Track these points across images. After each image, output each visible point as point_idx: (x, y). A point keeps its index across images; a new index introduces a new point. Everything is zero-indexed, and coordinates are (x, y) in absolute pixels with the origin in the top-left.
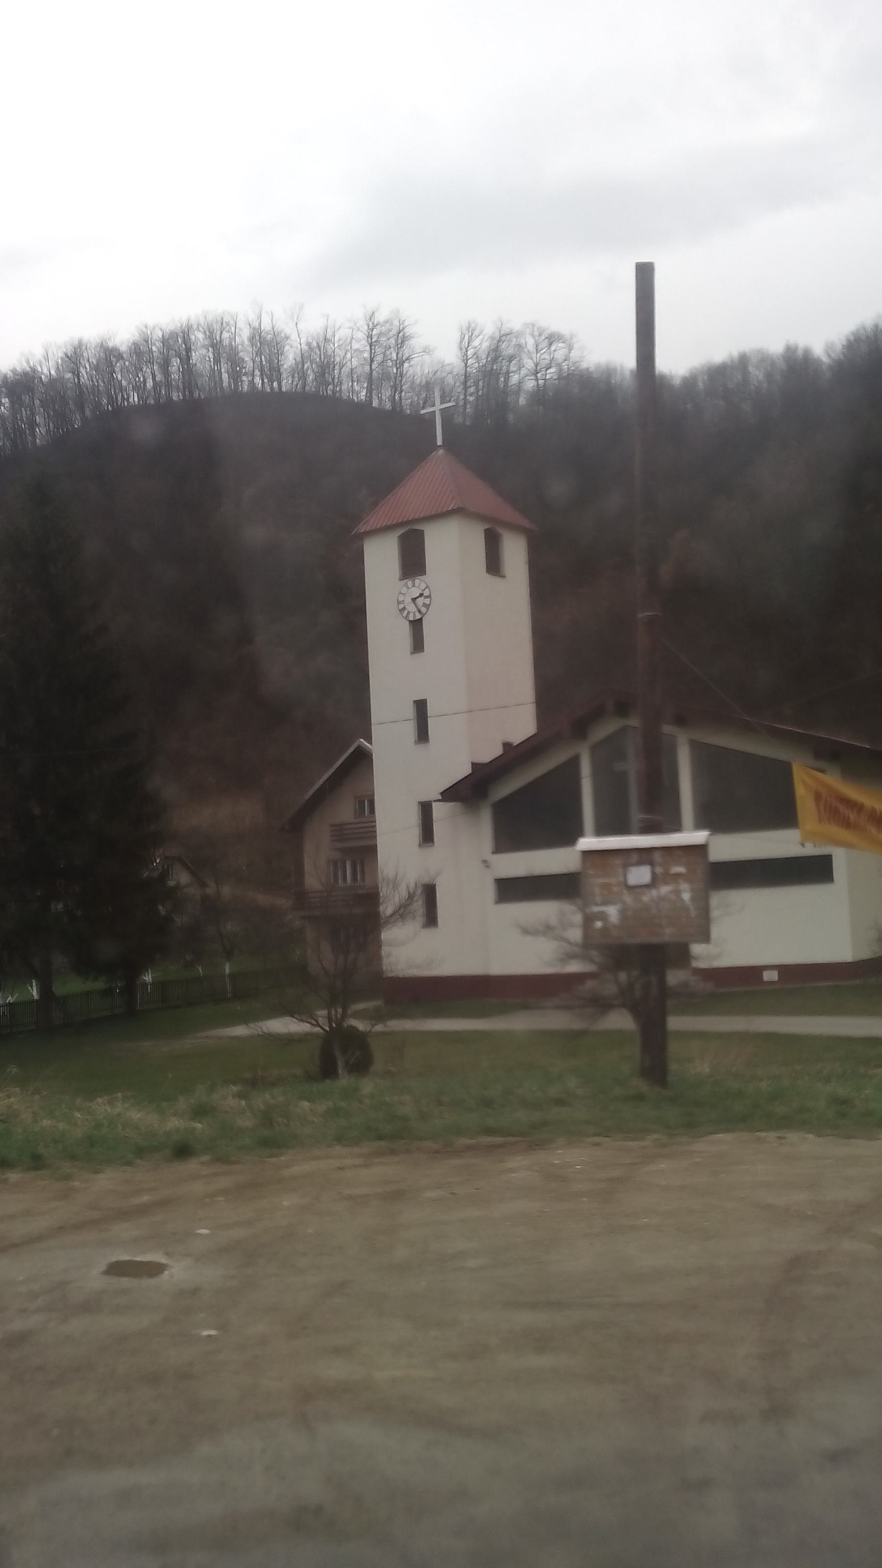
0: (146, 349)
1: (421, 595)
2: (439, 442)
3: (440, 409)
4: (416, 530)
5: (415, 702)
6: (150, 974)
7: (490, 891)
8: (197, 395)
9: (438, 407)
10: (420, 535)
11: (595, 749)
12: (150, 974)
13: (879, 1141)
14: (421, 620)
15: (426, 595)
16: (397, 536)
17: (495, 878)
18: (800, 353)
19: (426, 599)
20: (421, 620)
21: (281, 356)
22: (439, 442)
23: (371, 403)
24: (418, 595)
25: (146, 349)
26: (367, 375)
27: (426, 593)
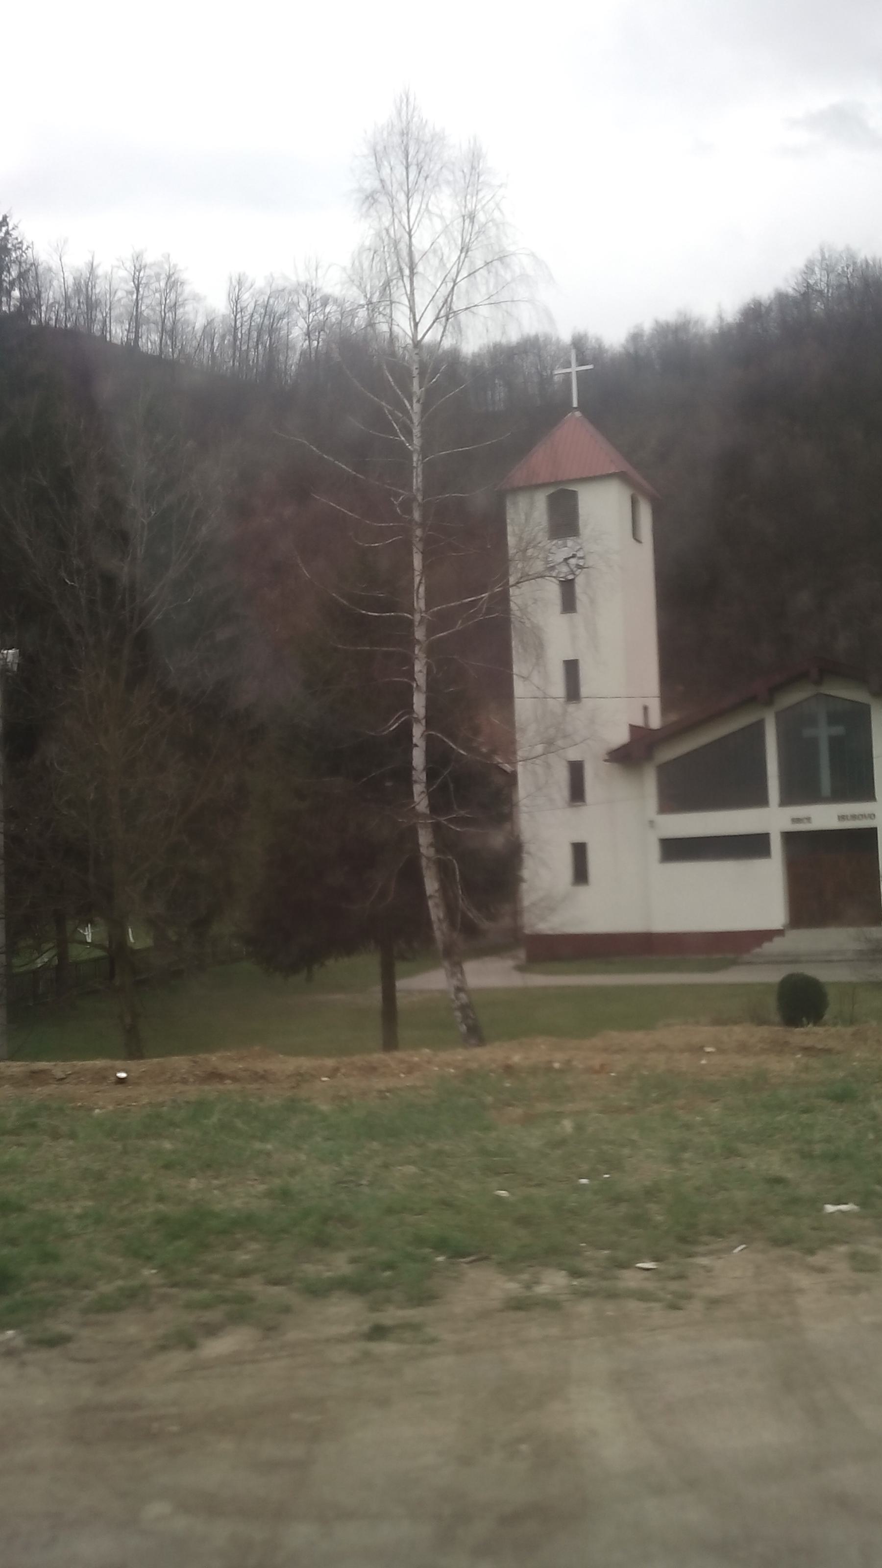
0: (75, 305)
1: (574, 556)
2: (575, 404)
3: (577, 371)
4: (567, 490)
5: (564, 661)
6: (89, 929)
7: (655, 851)
8: (556, 373)
9: (574, 369)
10: (573, 496)
11: (778, 716)
12: (89, 929)
13: (681, 1311)
14: (572, 580)
15: (580, 556)
16: (547, 494)
17: (792, 818)
18: (855, 282)
19: (580, 560)
20: (572, 580)
21: (285, 311)
22: (575, 404)
23: (142, 342)
24: (571, 555)
25: (75, 305)
26: (597, 347)
27: (580, 554)
